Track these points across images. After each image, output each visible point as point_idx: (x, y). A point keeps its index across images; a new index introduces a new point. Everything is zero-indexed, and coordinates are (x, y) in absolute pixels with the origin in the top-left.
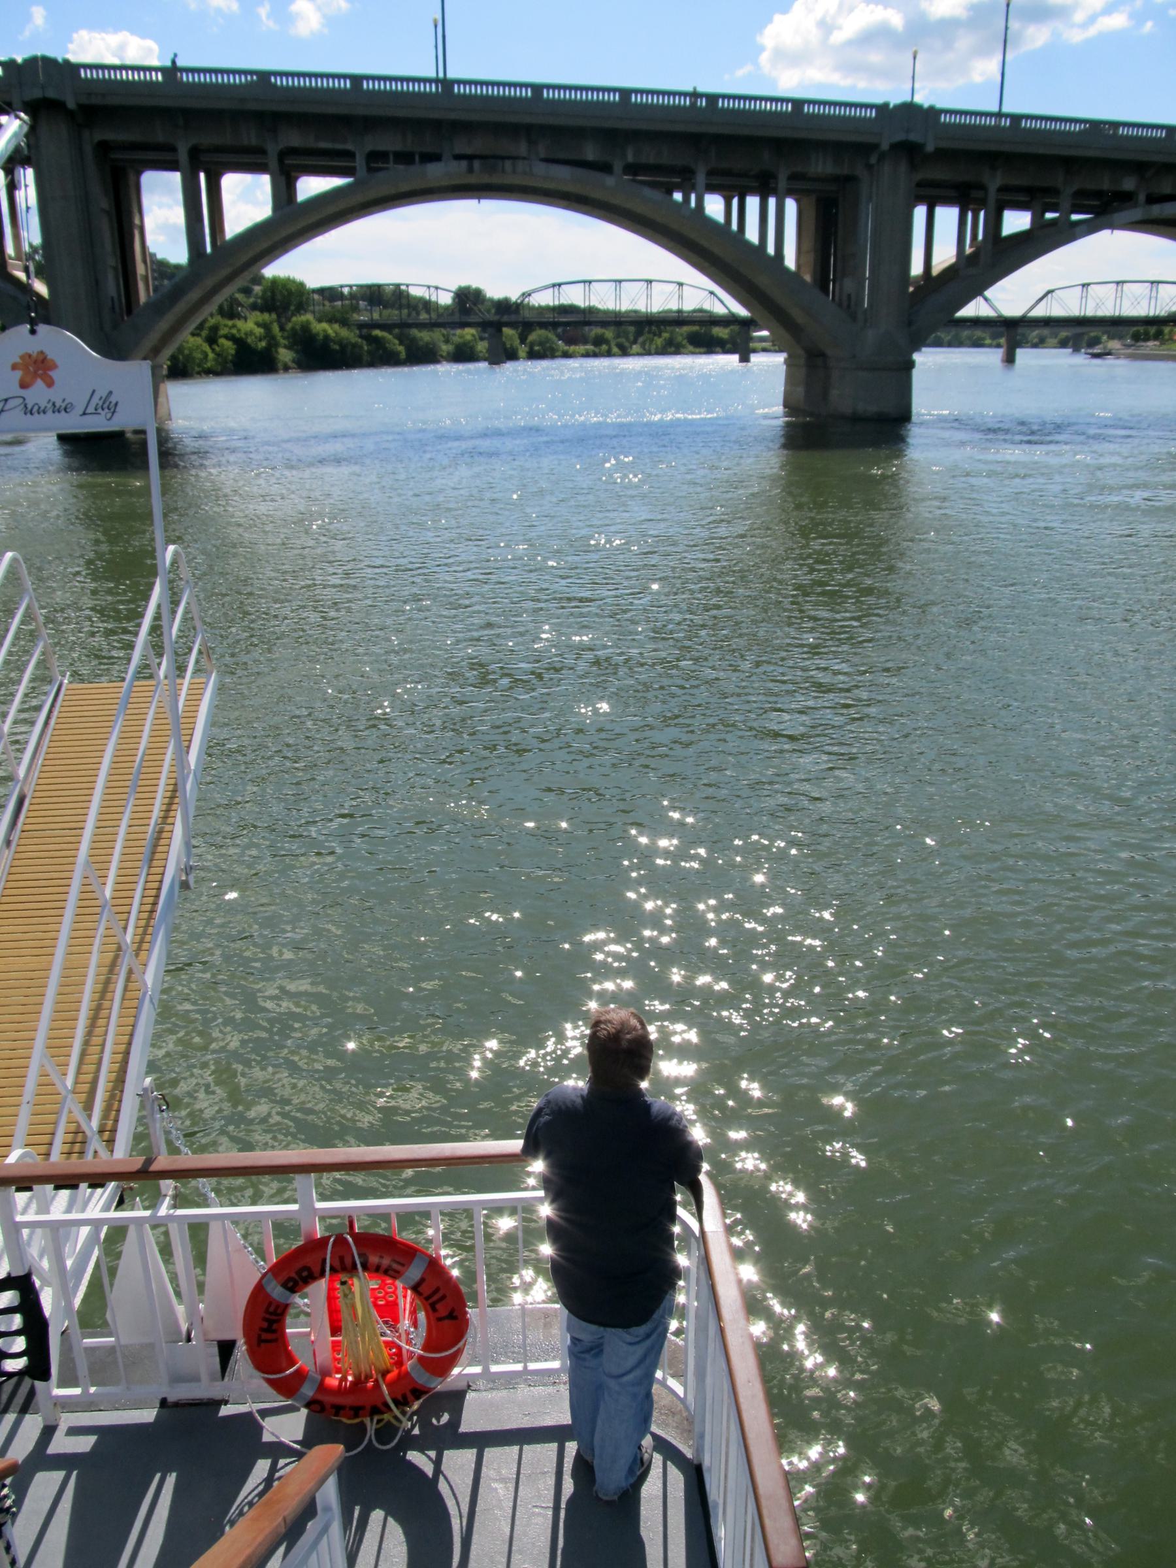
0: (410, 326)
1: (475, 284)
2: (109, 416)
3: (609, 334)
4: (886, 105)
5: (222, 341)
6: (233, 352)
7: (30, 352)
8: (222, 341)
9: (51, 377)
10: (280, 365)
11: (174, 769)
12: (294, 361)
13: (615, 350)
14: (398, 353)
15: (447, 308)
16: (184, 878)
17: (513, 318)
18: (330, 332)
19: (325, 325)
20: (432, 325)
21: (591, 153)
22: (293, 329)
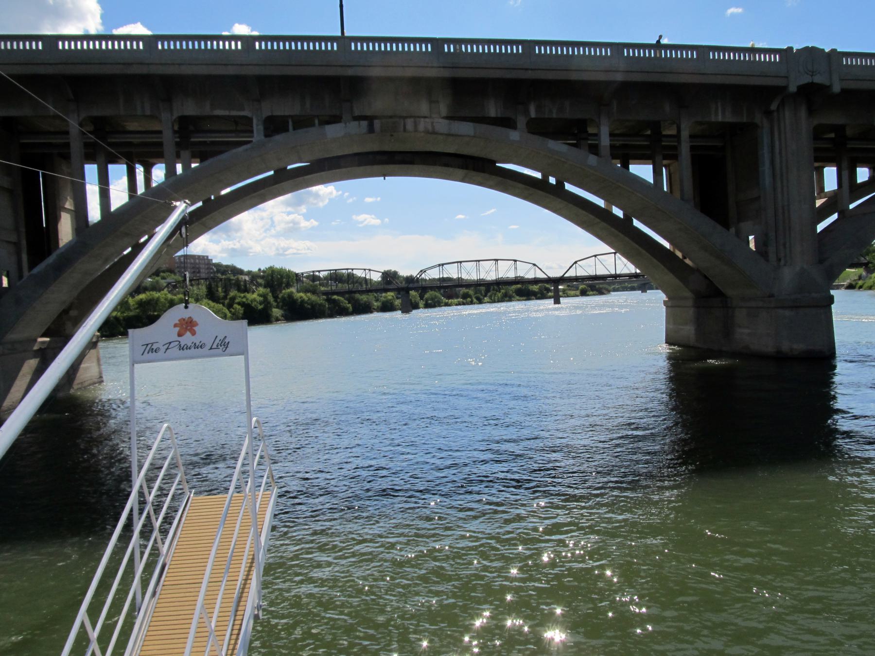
0: (355, 292)
1: (393, 268)
3: (471, 292)
5: (236, 306)
6: (242, 312)
8: (236, 306)
9: (194, 330)
11: (253, 545)
13: (475, 300)
14: (347, 309)
15: (378, 283)
16: (256, 613)
17: (416, 285)
19: (302, 294)
20: (368, 291)
22: (282, 297)
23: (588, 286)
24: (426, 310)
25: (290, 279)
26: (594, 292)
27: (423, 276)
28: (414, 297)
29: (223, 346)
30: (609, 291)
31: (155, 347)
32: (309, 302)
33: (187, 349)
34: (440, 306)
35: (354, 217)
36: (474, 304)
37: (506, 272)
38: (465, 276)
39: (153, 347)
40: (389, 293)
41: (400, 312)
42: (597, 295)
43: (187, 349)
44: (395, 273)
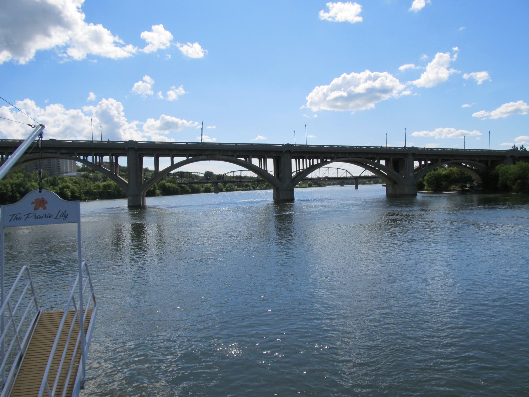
1: (210, 170)
2: (65, 219)
3: (250, 184)
4: (284, 144)
10: (157, 195)
12: (160, 193)
13: (252, 188)
14: (189, 191)
18: (170, 185)
19: (169, 184)
20: (198, 183)
21: (230, 154)
26: (316, 186)
29: (64, 217)
30: (324, 185)
31: (18, 216)
33: (40, 218)
36: (251, 190)
39: (17, 217)
40: (208, 184)
42: (318, 187)
44: (211, 173)
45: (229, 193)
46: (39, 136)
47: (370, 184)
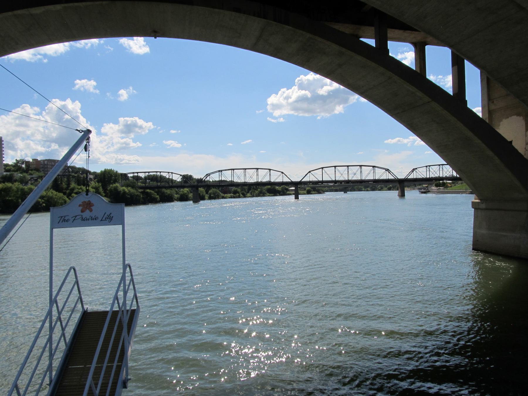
7: (86, 201)
9: (92, 209)
13: (241, 195)
17: (203, 184)
18: (126, 190)
19: (124, 188)
22: (110, 189)
23: (311, 188)
24: (209, 201)
25: (117, 178)
26: (315, 192)
27: (208, 178)
28: (202, 192)
30: (324, 192)
31: (66, 218)
32: (129, 193)
33: (86, 220)
34: (218, 198)
35: (164, 142)
36: (241, 197)
37: (263, 177)
38: (236, 180)
39: (65, 218)
41: (191, 202)
42: (317, 194)
43: (86, 220)
44: (191, 176)
45: (213, 201)
46: (86, 141)
47: (367, 190)
